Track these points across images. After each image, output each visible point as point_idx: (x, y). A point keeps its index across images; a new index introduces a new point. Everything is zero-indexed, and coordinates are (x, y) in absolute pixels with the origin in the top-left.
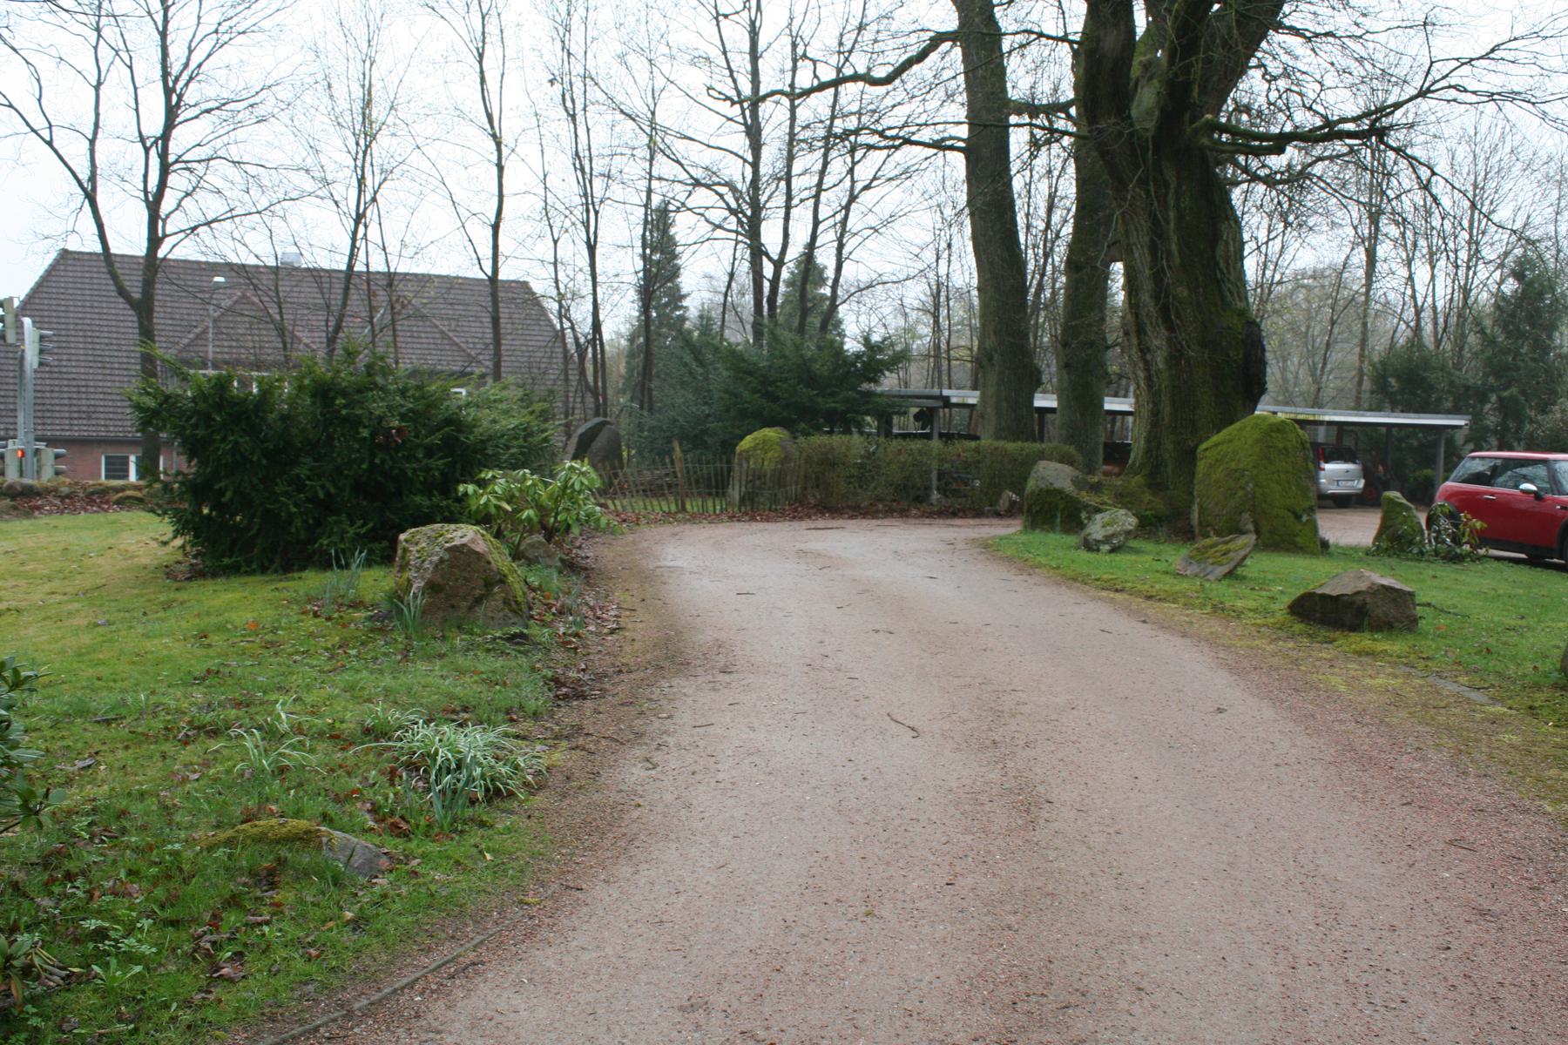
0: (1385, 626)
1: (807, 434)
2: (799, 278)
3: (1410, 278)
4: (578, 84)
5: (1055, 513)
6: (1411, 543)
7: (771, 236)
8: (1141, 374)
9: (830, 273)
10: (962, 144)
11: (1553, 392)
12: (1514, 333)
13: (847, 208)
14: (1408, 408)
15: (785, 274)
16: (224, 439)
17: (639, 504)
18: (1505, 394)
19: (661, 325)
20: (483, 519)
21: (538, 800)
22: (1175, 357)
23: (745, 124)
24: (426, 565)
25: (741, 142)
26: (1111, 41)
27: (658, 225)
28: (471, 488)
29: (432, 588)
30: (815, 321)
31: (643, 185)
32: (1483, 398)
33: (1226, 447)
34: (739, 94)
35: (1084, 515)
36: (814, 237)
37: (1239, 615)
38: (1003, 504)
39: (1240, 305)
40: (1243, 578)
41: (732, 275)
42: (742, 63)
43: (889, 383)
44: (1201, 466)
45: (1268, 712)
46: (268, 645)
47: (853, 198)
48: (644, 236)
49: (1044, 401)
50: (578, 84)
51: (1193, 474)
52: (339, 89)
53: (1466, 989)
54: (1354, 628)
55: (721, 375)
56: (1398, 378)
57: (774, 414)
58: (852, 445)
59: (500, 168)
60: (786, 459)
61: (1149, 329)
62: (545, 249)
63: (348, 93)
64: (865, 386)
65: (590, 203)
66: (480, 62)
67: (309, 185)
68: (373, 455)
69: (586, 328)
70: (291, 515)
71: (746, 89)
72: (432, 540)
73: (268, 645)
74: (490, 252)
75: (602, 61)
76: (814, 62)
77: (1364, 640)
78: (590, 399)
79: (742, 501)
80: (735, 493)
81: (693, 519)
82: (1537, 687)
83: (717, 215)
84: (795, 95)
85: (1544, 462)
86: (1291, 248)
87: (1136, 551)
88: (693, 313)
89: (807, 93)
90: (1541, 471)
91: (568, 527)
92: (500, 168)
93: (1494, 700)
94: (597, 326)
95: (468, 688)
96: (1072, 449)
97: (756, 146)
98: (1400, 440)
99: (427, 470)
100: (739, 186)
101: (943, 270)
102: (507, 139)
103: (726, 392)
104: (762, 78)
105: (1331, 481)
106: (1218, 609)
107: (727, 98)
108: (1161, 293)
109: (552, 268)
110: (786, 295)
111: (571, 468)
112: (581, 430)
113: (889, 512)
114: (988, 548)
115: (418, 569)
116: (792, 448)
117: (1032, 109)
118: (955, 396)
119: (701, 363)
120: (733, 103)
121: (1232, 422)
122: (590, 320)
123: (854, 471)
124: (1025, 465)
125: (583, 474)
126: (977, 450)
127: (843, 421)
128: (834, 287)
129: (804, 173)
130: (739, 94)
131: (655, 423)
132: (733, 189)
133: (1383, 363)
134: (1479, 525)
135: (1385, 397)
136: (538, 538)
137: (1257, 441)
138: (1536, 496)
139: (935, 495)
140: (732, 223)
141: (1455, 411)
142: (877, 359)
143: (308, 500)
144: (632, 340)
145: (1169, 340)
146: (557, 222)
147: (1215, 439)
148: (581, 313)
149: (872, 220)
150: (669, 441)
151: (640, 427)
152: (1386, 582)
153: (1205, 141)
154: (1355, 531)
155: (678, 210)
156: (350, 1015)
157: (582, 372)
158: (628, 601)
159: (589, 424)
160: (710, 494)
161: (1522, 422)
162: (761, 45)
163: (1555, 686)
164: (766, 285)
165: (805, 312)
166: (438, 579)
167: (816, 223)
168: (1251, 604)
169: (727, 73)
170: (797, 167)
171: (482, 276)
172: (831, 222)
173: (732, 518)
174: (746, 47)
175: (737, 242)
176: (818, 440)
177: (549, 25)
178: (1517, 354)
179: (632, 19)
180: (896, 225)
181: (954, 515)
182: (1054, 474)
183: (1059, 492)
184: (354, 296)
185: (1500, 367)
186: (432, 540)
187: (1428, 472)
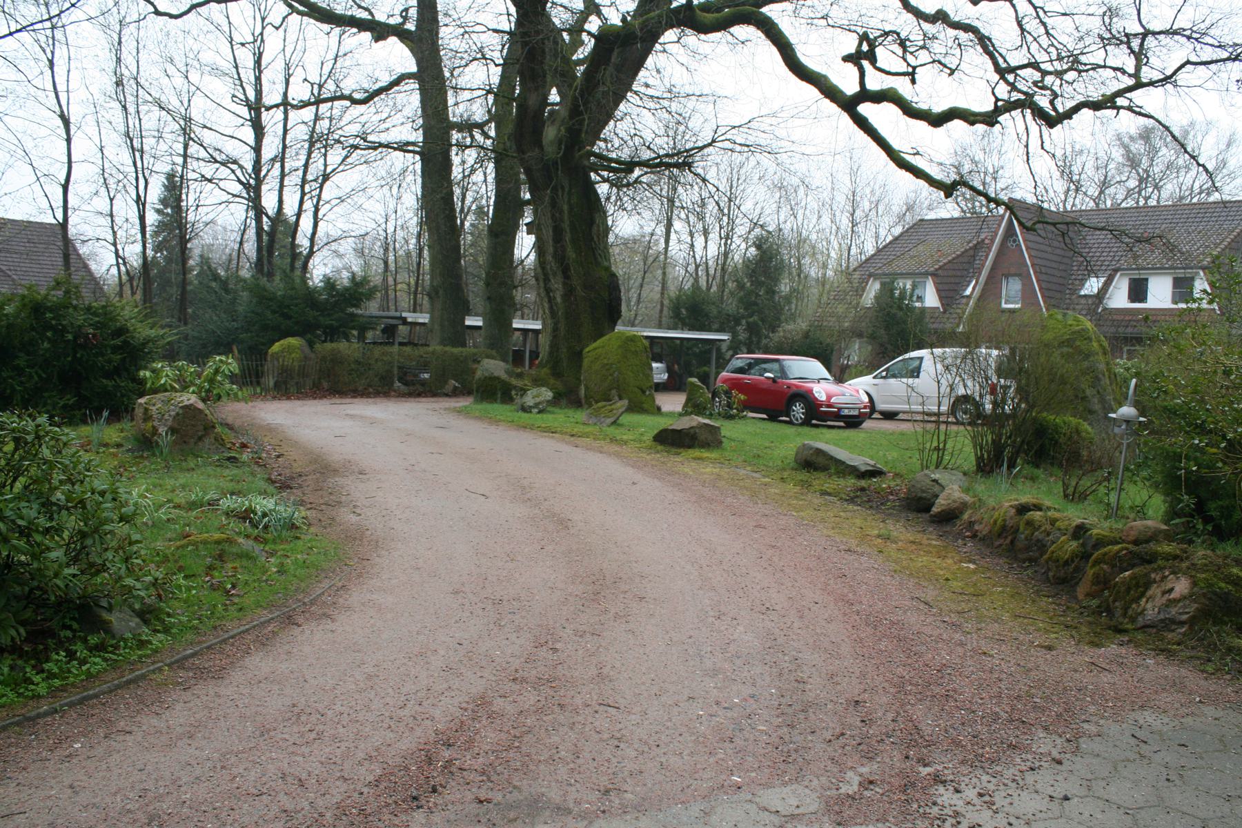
0: (706, 445)
3: (692, 246)
5: (494, 392)
6: (705, 408)
8: (546, 305)
12: (757, 283)
14: (693, 328)
18: (751, 320)
22: (569, 292)
24: (166, 417)
25: (248, 134)
28: (148, 374)
29: (173, 430)
32: (738, 322)
33: (600, 350)
35: (513, 393)
37: (626, 443)
39: (606, 264)
40: (621, 425)
42: (248, 76)
44: (586, 362)
45: (657, 483)
51: (580, 367)
53: (770, 569)
54: (690, 447)
56: (687, 309)
58: (347, 348)
59: (69, 140)
61: (551, 277)
62: (102, 204)
64: (353, 310)
68: (76, 353)
71: (251, 95)
75: (150, 72)
77: (696, 453)
79: (276, 384)
82: (784, 469)
87: (553, 413)
90: (776, 366)
92: (69, 140)
93: (764, 476)
99: (110, 361)
103: (253, 312)
106: (613, 440)
108: (561, 258)
111: (221, 361)
114: (459, 411)
115: (160, 420)
121: (601, 335)
127: (333, 333)
133: (678, 298)
134: (742, 397)
135: (678, 321)
137: (620, 347)
138: (774, 380)
141: (720, 330)
145: (564, 284)
146: (112, 186)
153: (586, 163)
154: (672, 403)
156: (304, 604)
161: (760, 338)
163: (793, 469)
166: (176, 426)
171: (54, 222)
178: (757, 295)
181: (419, 395)
182: (494, 367)
183: (498, 378)
185: (749, 303)
187: (706, 368)
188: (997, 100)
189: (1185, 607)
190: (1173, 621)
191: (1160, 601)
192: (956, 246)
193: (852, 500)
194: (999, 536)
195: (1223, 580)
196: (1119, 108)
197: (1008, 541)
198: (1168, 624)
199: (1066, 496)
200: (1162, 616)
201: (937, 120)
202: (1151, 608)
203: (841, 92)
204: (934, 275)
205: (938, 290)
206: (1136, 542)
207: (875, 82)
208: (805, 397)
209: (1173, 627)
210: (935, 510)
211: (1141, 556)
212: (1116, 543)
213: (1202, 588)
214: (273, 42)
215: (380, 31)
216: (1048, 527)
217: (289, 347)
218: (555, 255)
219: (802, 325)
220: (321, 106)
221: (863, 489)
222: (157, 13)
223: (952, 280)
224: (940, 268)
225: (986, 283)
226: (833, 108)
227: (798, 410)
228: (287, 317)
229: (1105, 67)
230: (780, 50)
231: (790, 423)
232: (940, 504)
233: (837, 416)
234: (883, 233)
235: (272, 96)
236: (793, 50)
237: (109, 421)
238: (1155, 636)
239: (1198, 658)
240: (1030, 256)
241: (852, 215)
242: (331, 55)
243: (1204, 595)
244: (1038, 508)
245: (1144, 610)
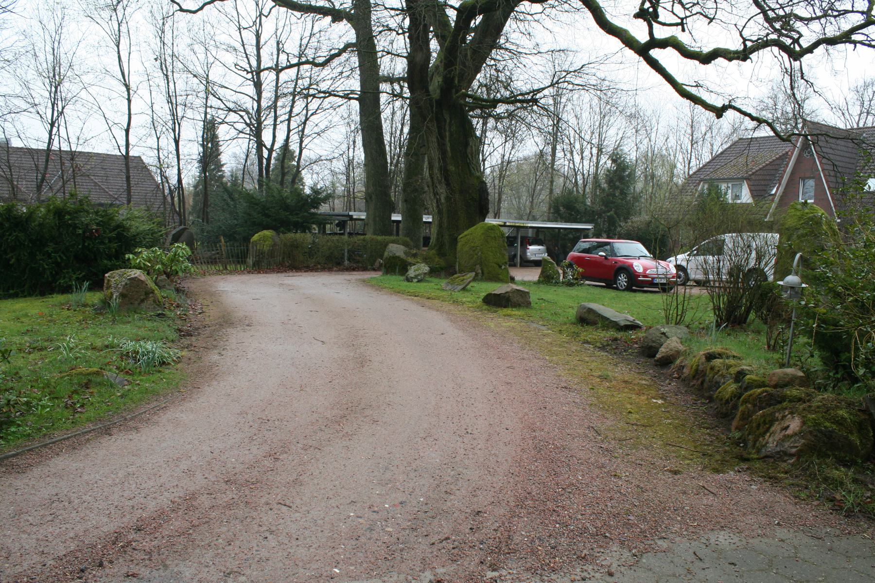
0: (517, 305)
1: (284, 233)
2: (281, 157)
4: (169, 60)
5: (397, 267)
6: (553, 278)
7: (267, 137)
9: (297, 153)
10: (356, 96)
11: (629, 213)
13: (305, 123)
14: (567, 221)
15: (274, 155)
16: (10, 235)
17: (204, 267)
19: (211, 179)
20: (139, 267)
21: (179, 366)
23: (254, 81)
25: (251, 90)
26: (419, 57)
27: (210, 128)
28: (131, 256)
29: (123, 295)
30: (289, 178)
31: (202, 110)
34: (251, 67)
36: (288, 137)
38: (377, 264)
40: (467, 290)
41: (247, 156)
42: (252, 50)
43: (324, 208)
44: (459, 245)
45: (461, 334)
46: (50, 321)
47: (307, 119)
48: (203, 136)
49: (396, 217)
50: (169, 60)
51: (456, 249)
52: (42, 57)
54: (505, 307)
55: (242, 206)
57: (266, 222)
59: (129, 101)
60: (275, 245)
63: (45, 58)
64: (313, 210)
65: (176, 120)
66: (118, 46)
67: (24, 106)
68: (84, 242)
69: (174, 181)
70: (45, 269)
71: (254, 63)
72: (121, 276)
73: (50, 321)
74: (124, 143)
75: (182, 48)
76: (288, 54)
77: (508, 311)
78: (176, 218)
79: (254, 265)
80: (250, 261)
81: (231, 273)
82: (565, 324)
83: (241, 126)
84: (278, 69)
85: (608, 243)
86: (499, 150)
87: (428, 281)
88: (228, 174)
89: (283, 69)
91: (177, 272)
92: (129, 101)
93: (549, 329)
94: (180, 181)
95: (142, 332)
96: (408, 239)
97: (259, 93)
98: (565, 235)
100: (251, 111)
101: (351, 155)
102: (133, 86)
103: (245, 213)
104: (262, 59)
105: (532, 254)
106: (455, 302)
107: (245, 70)
109: (156, 152)
110: (275, 164)
111: (178, 247)
112: (174, 232)
113: (323, 269)
115: (115, 288)
116: (277, 240)
117: (391, 80)
118: (355, 215)
119: (233, 199)
120: (248, 72)
122: (176, 177)
123: (307, 250)
124: (385, 245)
125: (184, 249)
126: (364, 240)
127: (303, 227)
128: (298, 162)
129: (283, 107)
130: (251, 67)
131: (210, 229)
132: (248, 113)
134: (581, 270)
136: (164, 277)
138: (606, 257)
139: (346, 262)
140: (248, 130)
142: (318, 197)
143: (53, 263)
144: (196, 187)
146: (159, 129)
147: (466, 233)
148: (172, 174)
149: (316, 130)
150: (217, 237)
151: (202, 231)
152: (518, 288)
153: (462, 102)
155: (221, 123)
156: (126, 419)
157: (173, 204)
158: (206, 303)
159: (178, 229)
160: (238, 262)
162: (262, 41)
164: (265, 161)
165: (284, 175)
166: (125, 292)
167: (289, 131)
168: (469, 300)
169: (244, 55)
170: (279, 104)
172: (296, 130)
173: (249, 272)
174: (254, 43)
175: (250, 140)
176: (290, 235)
177: (153, 28)
179: (196, 28)
180: (328, 132)
181: (354, 270)
182: (396, 249)
183: (398, 257)
184: (51, 165)
186: (121, 276)
188: (745, 40)
189: (795, 442)
190: (786, 453)
191: (779, 436)
192: (768, 156)
193: (603, 348)
194: (694, 377)
195: (828, 420)
196: (855, 43)
197: (699, 382)
198: (782, 455)
199: (769, 347)
200: (778, 449)
201: (706, 58)
202: (771, 442)
203: (637, 41)
204: (747, 179)
205: (751, 191)
206: (775, 386)
207: (660, 33)
208: (628, 270)
209: (786, 458)
210: (658, 356)
211: (774, 398)
212: (759, 386)
213: (809, 427)
214: (268, 28)
215: (337, 15)
216: (724, 372)
217: (264, 237)
218: (440, 168)
219: (645, 217)
220: (302, 67)
221: (616, 339)
222: (181, 10)
223: (763, 183)
224: (753, 174)
225: (787, 185)
226: (630, 54)
227: (622, 279)
228: (267, 216)
229: (853, 11)
230: (592, 12)
231: (617, 289)
232: (662, 351)
233: (652, 284)
234: (715, 148)
235: (266, 62)
236: (601, 12)
237: (90, 289)
238: (768, 466)
239: (798, 486)
240: (820, 163)
241: (692, 135)
242: (307, 34)
243: (811, 433)
244: (720, 356)
245: (767, 443)
